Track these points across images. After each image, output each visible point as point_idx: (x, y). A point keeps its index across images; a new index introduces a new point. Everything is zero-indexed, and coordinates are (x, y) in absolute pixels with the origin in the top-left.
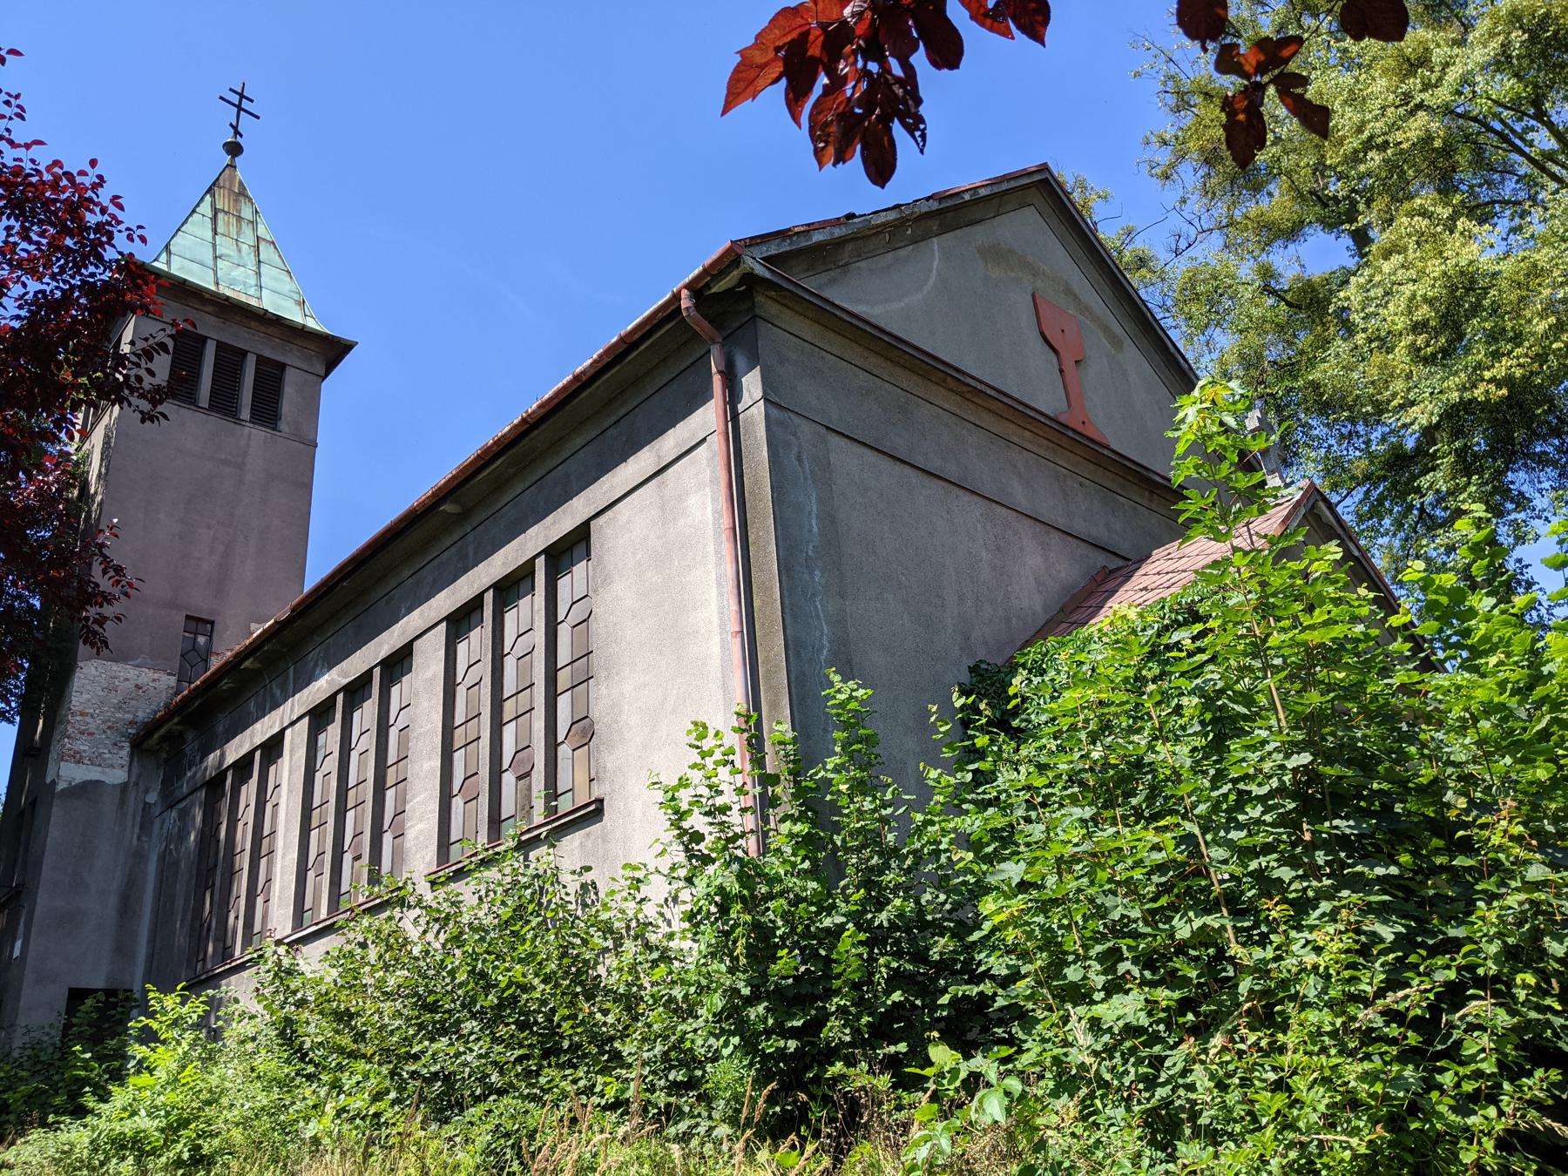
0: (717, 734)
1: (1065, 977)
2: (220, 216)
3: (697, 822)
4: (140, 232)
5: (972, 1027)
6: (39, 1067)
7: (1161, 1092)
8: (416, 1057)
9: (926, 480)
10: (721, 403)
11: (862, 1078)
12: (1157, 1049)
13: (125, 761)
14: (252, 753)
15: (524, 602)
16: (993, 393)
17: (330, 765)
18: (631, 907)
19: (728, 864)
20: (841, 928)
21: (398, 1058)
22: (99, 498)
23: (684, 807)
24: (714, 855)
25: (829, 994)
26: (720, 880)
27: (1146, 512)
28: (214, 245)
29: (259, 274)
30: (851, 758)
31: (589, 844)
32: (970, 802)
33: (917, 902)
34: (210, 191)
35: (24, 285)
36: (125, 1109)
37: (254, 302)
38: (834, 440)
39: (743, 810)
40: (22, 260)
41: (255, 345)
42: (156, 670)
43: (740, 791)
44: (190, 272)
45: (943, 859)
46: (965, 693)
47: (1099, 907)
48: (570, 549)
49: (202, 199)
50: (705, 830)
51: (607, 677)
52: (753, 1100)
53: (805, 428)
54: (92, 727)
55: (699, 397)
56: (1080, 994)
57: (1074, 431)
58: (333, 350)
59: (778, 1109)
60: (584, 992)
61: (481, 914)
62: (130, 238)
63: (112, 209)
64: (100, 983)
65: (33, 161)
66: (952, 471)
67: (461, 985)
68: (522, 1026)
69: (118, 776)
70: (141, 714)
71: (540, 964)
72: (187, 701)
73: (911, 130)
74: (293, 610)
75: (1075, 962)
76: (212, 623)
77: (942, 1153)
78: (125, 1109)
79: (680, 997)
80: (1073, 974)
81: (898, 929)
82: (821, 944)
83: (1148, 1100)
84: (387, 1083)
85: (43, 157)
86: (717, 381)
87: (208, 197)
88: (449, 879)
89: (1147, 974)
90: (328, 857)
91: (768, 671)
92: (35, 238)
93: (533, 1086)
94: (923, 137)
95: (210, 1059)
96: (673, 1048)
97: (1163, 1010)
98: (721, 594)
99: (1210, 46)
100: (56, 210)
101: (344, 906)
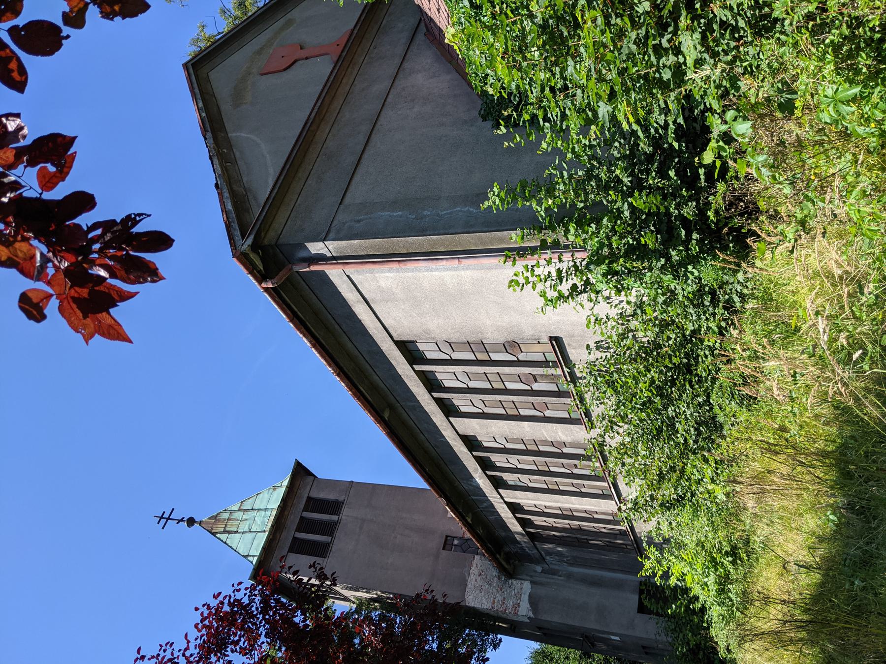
0: (516, 275)
1: (669, 80)
2: (227, 529)
3: (565, 288)
4: (236, 585)
5: (695, 133)
6: (678, 629)
7: (742, 23)
8: (685, 440)
9: (371, 144)
10: (326, 266)
11: (717, 200)
12: (715, 27)
13: (519, 582)
14: (517, 518)
15: (439, 376)
16: (320, 102)
17: (525, 479)
18: (611, 323)
19: (590, 271)
20: (631, 205)
21: (685, 450)
22: (379, 593)
23: (556, 294)
24: (585, 278)
25: (668, 214)
26: (599, 276)
27: (392, 7)
28: (244, 532)
29: (259, 510)
30: (534, 196)
31: (574, 344)
32: (562, 124)
33: (618, 159)
34: (214, 534)
35: (263, 643)
36: (703, 589)
37: (274, 513)
38: (347, 200)
39: (560, 261)
40: (249, 644)
41: (297, 512)
42: (471, 565)
43: (549, 262)
44: (258, 545)
45: (594, 143)
46: (498, 126)
47: (628, 58)
48: (410, 351)
49: (219, 539)
50: (570, 282)
51: (482, 333)
52: (724, 260)
53: (340, 217)
54: (500, 598)
55: (323, 276)
56: (679, 71)
57: (342, 52)
58: (300, 472)
59: (731, 245)
60: (656, 349)
61: (610, 403)
62: (239, 590)
63: (221, 598)
64: (636, 597)
65: (196, 639)
66: (365, 128)
67: (648, 416)
68: (673, 384)
69: (527, 586)
70: (494, 574)
71: (639, 373)
72: (488, 550)
73: (136, 223)
74: (441, 496)
75: (660, 73)
76: (447, 536)
77: (766, 160)
78: (703, 589)
79: (663, 298)
80: (667, 75)
81: (633, 171)
82: (639, 218)
83: (745, 31)
84: (699, 456)
85: (193, 634)
86: (314, 268)
87: (218, 535)
88: (590, 420)
89: (670, 29)
90: (575, 481)
91: (481, 243)
92: (237, 638)
93: (706, 379)
94: (140, 215)
95: (680, 545)
96: (692, 304)
97: (693, 22)
98: (437, 270)
99: (64, 34)
100: (224, 625)
101: (601, 474)
